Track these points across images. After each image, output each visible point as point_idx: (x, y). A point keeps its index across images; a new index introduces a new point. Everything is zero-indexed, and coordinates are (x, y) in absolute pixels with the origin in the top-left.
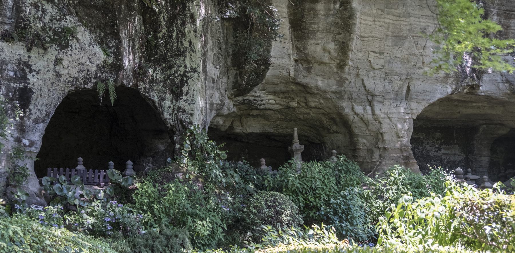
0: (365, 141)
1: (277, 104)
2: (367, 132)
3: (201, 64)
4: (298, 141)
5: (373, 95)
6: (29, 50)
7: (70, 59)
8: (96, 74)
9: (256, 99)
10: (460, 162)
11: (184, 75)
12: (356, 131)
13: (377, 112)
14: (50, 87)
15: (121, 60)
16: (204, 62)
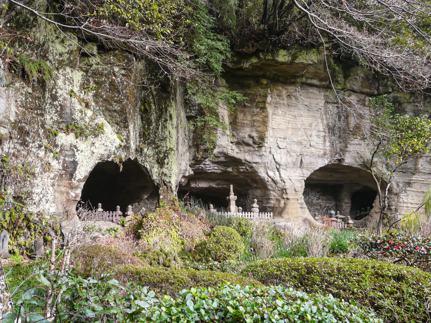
0: (275, 194)
1: (219, 169)
2: (276, 188)
3: (176, 145)
4: (233, 193)
5: (280, 165)
6: (77, 138)
7: (100, 143)
8: (114, 152)
9: (206, 166)
10: (332, 207)
11: (165, 152)
12: (269, 187)
13: (282, 175)
14: (87, 160)
15: (130, 143)
16: (177, 143)
